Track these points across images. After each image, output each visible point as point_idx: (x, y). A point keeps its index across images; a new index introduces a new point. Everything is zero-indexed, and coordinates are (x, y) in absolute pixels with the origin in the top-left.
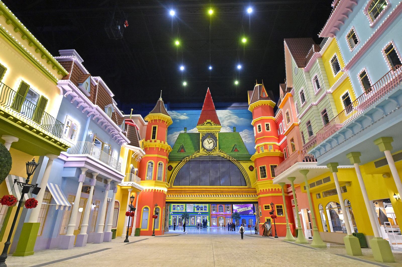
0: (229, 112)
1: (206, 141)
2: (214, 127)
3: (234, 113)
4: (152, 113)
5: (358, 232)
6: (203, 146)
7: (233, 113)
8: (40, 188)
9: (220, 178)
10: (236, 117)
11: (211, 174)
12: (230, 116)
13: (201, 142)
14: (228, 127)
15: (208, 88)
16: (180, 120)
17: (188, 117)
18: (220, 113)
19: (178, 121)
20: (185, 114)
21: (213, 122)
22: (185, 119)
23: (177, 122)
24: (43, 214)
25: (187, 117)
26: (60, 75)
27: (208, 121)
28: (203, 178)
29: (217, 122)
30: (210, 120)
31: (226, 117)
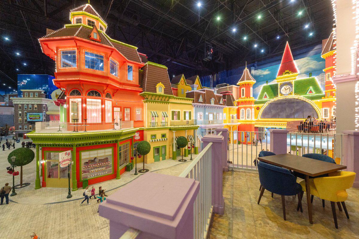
0: (307, 59)
1: (283, 88)
2: (291, 74)
3: (313, 59)
4: (240, 81)
5: (59, 89)
6: (280, 93)
7: (311, 59)
8: (331, 202)
9: (294, 114)
10: (315, 62)
11: (288, 111)
12: (308, 62)
13: (279, 90)
14: (304, 74)
15: (287, 42)
16: (264, 75)
17: (270, 72)
18: (296, 63)
19: (262, 76)
20: (267, 70)
21: (291, 71)
22: (267, 74)
23: (262, 77)
24: (120, 209)
25: (269, 72)
26: (227, 177)
27: (286, 71)
28: (281, 114)
29: (293, 70)
30: (289, 70)
31: (304, 64)
